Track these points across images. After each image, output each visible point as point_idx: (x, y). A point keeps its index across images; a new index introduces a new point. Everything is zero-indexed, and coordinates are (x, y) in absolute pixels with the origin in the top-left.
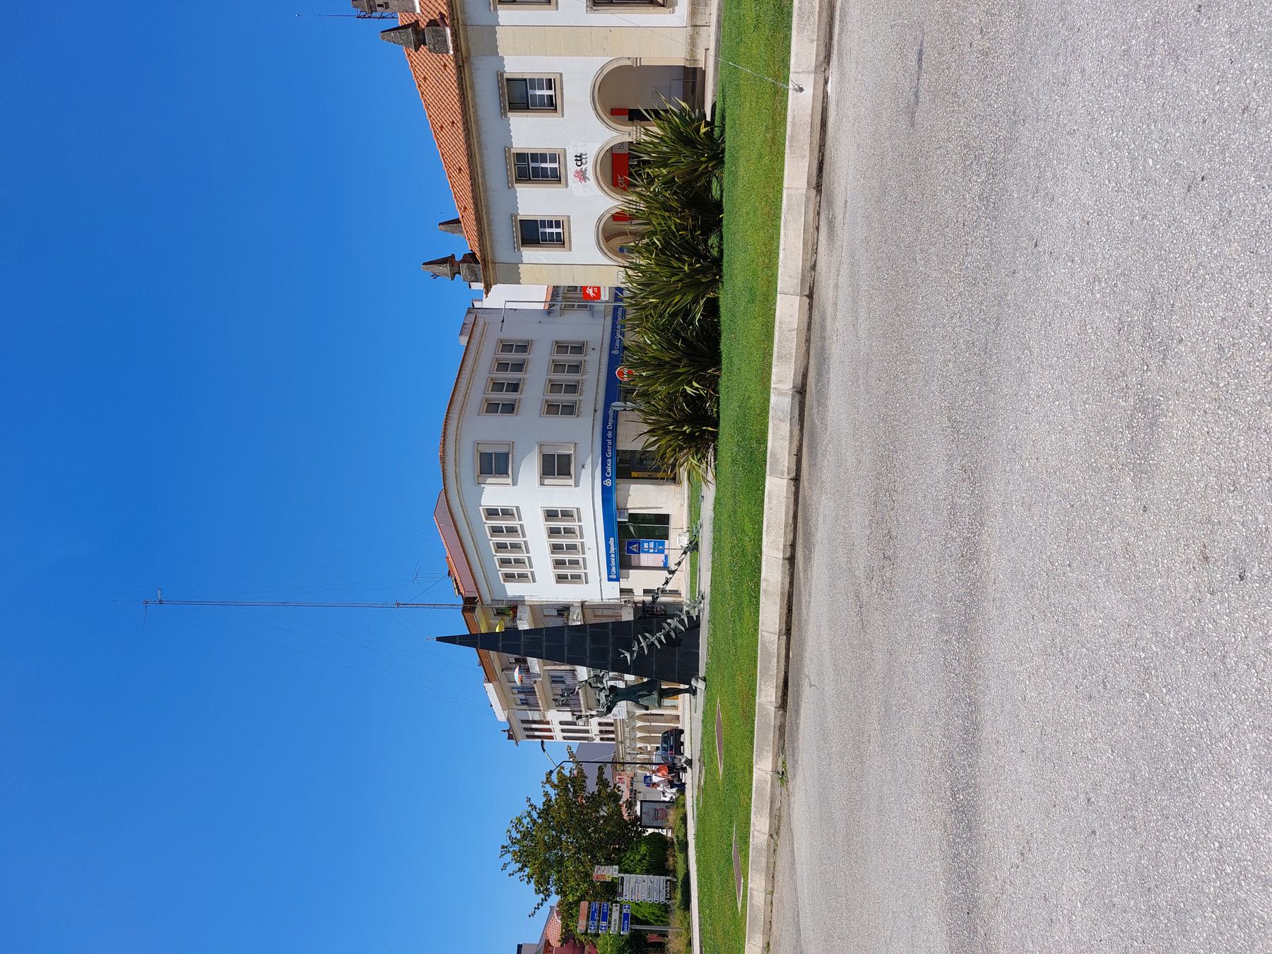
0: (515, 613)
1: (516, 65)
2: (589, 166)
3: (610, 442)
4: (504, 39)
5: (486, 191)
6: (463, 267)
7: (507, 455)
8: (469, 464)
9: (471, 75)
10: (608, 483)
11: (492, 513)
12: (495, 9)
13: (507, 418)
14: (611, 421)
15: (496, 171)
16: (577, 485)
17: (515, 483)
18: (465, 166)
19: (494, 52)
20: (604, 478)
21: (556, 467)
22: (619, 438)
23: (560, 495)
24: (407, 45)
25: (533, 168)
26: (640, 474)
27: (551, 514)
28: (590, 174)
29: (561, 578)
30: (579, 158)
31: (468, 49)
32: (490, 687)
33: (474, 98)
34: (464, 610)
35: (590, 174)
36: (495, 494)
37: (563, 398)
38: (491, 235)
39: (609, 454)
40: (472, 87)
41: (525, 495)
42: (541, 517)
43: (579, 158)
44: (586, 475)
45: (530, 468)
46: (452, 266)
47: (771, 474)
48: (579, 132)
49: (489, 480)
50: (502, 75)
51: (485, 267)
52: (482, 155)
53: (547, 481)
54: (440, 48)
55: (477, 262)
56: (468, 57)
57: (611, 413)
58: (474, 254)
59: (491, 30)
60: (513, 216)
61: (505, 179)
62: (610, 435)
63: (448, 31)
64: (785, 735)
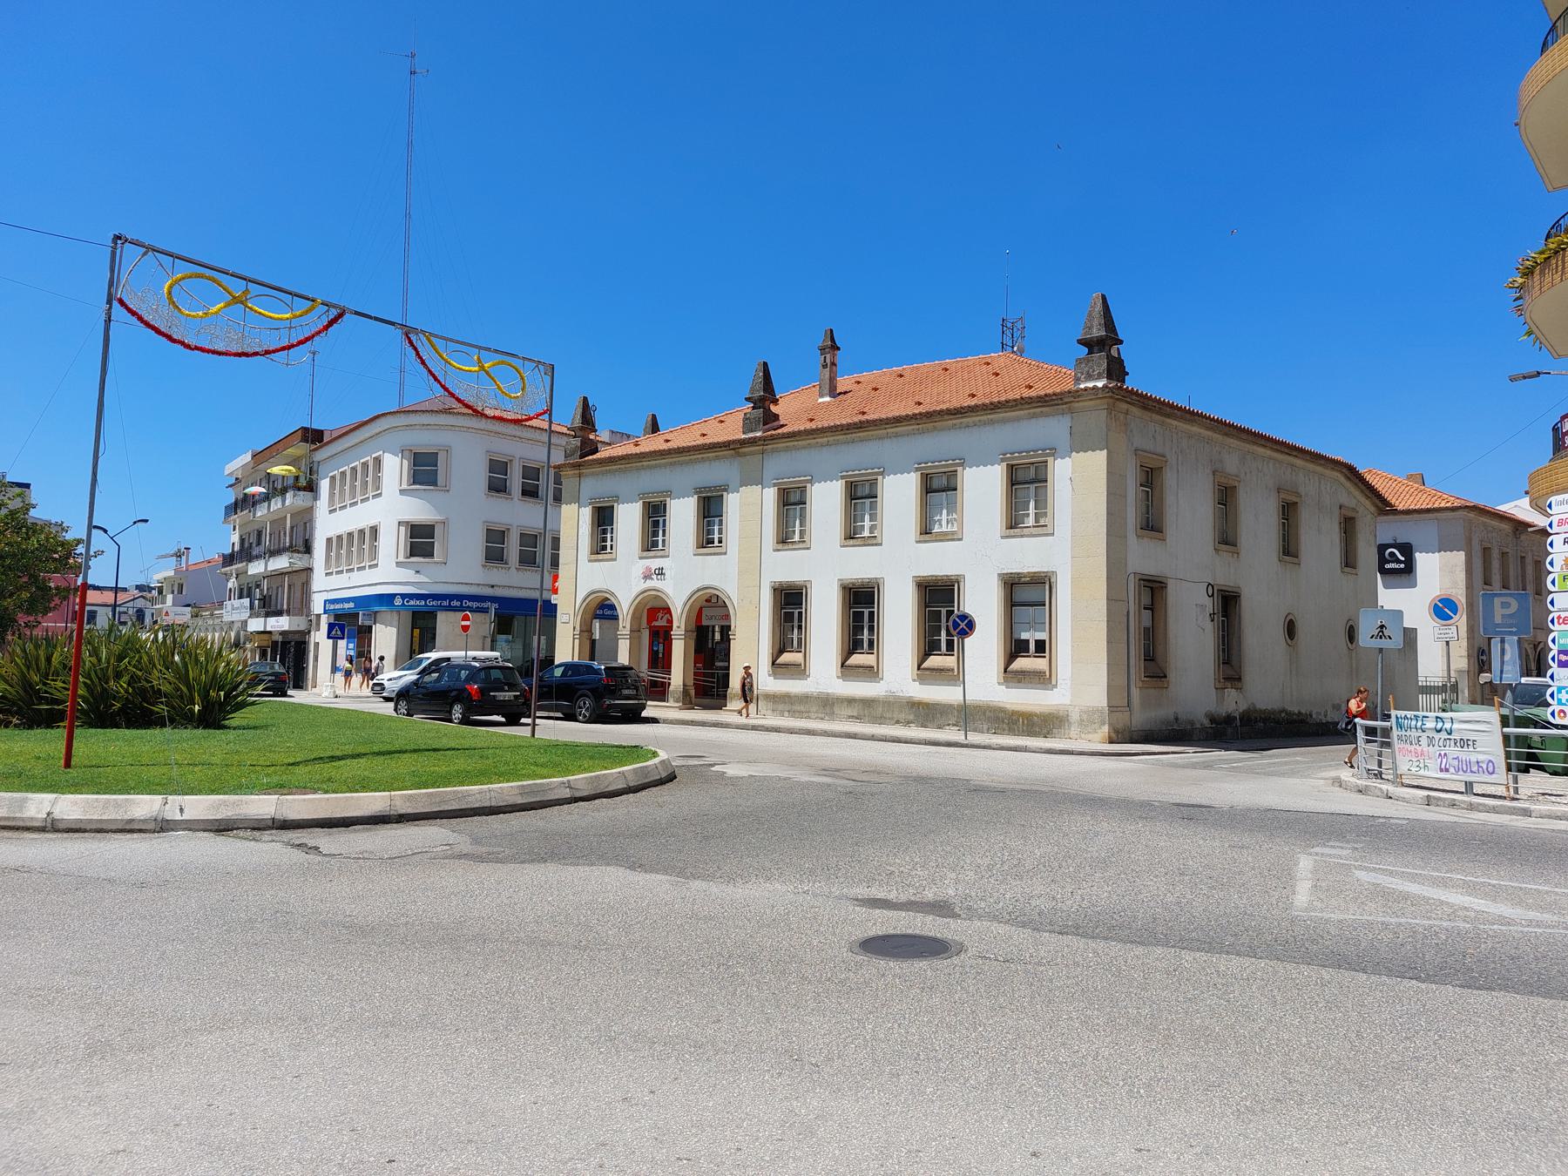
0: (304, 489)
1: (733, 503)
2: (654, 583)
3: (446, 603)
4: (752, 492)
5: (638, 469)
6: (577, 442)
7: (435, 483)
8: (425, 440)
9: (725, 457)
10: (398, 602)
11: (378, 461)
12: (917, 470)
13: (483, 483)
14: (475, 605)
15: (936, 446)
16: (398, 564)
17: (402, 492)
18: (707, 440)
19: (744, 483)
20: (403, 596)
21: (420, 540)
22: (451, 614)
23: (391, 544)
24: (752, 390)
25: (938, 487)
26: (416, 640)
27: (374, 530)
28: (650, 584)
29: (329, 540)
30: (660, 572)
31: (745, 455)
32: (247, 457)
33: (709, 459)
34: (305, 430)
35: (650, 584)
36: (394, 468)
37: (513, 549)
38: (603, 473)
39: (431, 603)
40: (717, 458)
41: (391, 506)
42: (372, 523)
43: (660, 572)
44: (407, 575)
45: (418, 509)
46: (581, 429)
47: (21, 811)
48: (682, 576)
49: (405, 462)
50: (962, 465)
51: (578, 466)
52: (665, 466)
53: (402, 529)
54: (748, 425)
55: (582, 457)
56: (739, 455)
57: (485, 605)
58: (596, 451)
59: (760, 481)
60: (617, 499)
61: (1026, 447)
62: (455, 603)
63: (759, 434)
64: (222, 828)
